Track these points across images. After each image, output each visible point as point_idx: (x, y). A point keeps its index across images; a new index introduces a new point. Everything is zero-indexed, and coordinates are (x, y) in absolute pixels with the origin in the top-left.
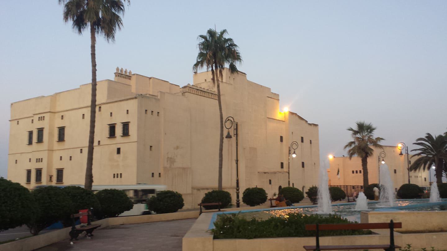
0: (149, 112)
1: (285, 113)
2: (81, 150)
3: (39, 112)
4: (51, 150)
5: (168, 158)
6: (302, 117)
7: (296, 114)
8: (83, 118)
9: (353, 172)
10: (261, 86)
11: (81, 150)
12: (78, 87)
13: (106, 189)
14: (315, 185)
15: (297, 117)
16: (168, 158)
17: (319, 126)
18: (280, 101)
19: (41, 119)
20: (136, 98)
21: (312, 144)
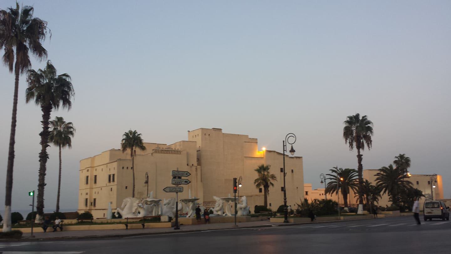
0: (125, 168)
1: (264, 152)
2: (101, 188)
3: (62, 176)
4: (91, 188)
5: (138, 192)
6: (280, 152)
7: (274, 152)
8: (102, 171)
9: (320, 195)
10: (238, 135)
11: (101, 188)
12: (101, 153)
13: (15, 212)
14: (387, 205)
15: (276, 154)
16: (138, 192)
17: (303, 158)
18: (258, 143)
19: (88, 171)
20: (116, 161)
21: (294, 173)
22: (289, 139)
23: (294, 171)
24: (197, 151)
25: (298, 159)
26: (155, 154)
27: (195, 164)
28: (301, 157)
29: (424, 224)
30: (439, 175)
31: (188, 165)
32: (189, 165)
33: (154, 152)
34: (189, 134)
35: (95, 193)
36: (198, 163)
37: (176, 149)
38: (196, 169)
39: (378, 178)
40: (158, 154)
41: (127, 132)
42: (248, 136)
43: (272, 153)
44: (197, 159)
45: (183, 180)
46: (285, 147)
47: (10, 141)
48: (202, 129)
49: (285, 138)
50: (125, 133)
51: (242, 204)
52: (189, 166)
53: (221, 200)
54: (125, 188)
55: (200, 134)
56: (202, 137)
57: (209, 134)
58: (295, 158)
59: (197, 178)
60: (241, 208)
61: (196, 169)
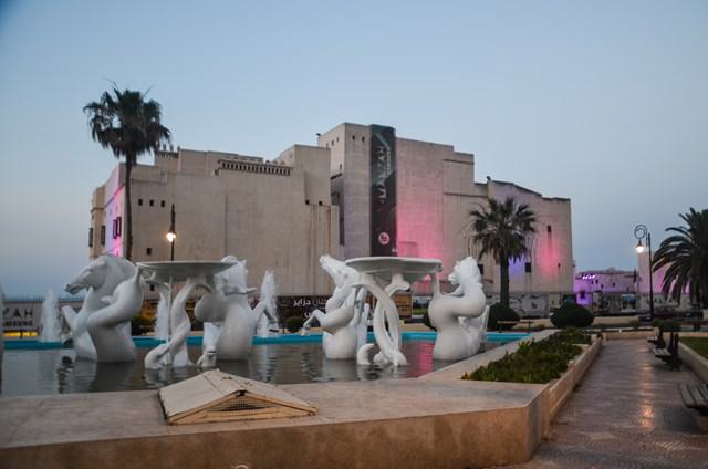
7: (512, 184)
15: (514, 189)
24: (332, 178)
26: (224, 171)
27: (327, 200)
29: (669, 441)
31: (307, 202)
35: (140, 202)
38: (329, 211)
39: (668, 273)
40: (237, 173)
41: (696, 211)
43: (508, 186)
44: (332, 194)
45: (691, 320)
47: (395, 210)
48: (346, 124)
50: (690, 213)
53: (352, 272)
55: (342, 140)
60: (454, 317)
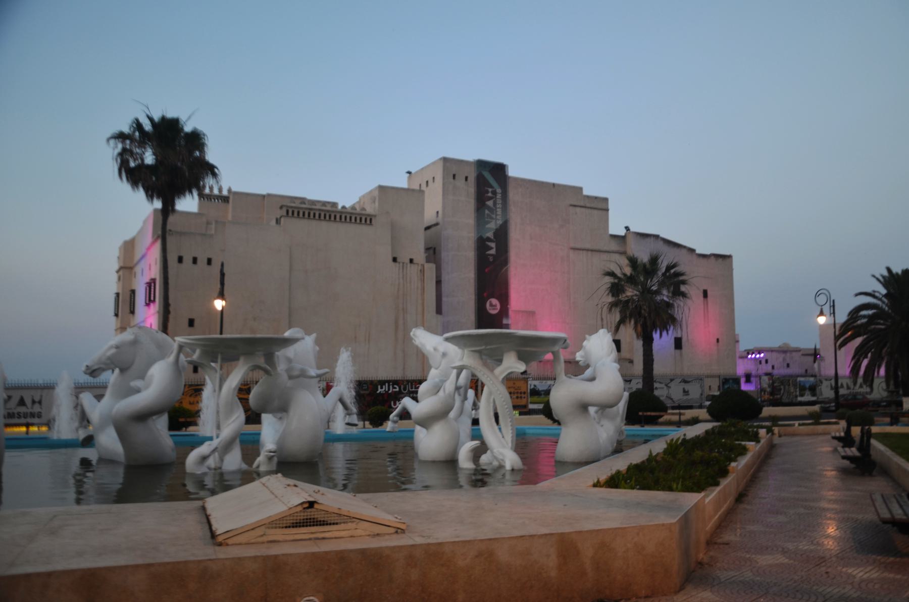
7: (657, 237)
22: (826, 301)
23: (709, 293)
25: (720, 260)
27: (420, 256)
28: (730, 257)
30: (266, 412)
32: (398, 260)
33: (285, 214)
34: (409, 178)
36: (426, 257)
37: (356, 209)
38: (422, 271)
42: (581, 189)
46: (832, 312)
49: (815, 293)
51: (592, 379)
52: (397, 264)
54: (186, 322)
56: (444, 184)
57: (454, 173)
58: (713, 257)
59: (423, 300)
61: (422, 271)
